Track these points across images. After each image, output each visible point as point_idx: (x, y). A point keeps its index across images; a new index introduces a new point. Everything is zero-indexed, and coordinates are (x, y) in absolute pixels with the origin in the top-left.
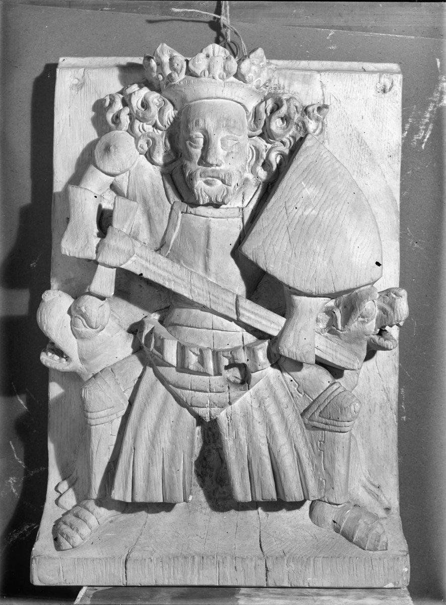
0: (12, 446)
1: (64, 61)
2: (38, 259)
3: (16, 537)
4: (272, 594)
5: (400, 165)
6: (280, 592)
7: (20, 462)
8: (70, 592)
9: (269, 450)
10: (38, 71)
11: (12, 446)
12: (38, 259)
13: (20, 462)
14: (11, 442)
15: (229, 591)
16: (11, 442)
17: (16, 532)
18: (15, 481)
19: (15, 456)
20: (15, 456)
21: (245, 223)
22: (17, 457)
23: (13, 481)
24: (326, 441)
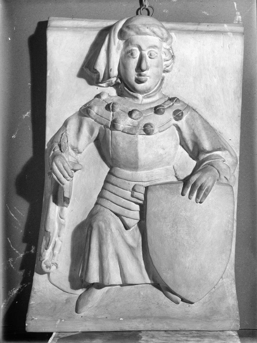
0: (9, 240)
1: (54, 22)
2: (16, 133)
3: (15, 292)
4: (160, 340)
5: (241, 101)
6: (165, 339)
7: (14, 249)
8: (48, 335)
9: (60, 129)
10: (32, 31)
11: (9, 240)
12: (16, 133)
13: (14, 249)
14: (8, 238)
15: (135, 335)
16: (8, 238)
17: (15, 289)
18: (12, 260)
19: (11, 246)
20: (11, 246)
21: (145, 134)
22: (12, 246)
23: (11, 261)
24: (213, 287)
